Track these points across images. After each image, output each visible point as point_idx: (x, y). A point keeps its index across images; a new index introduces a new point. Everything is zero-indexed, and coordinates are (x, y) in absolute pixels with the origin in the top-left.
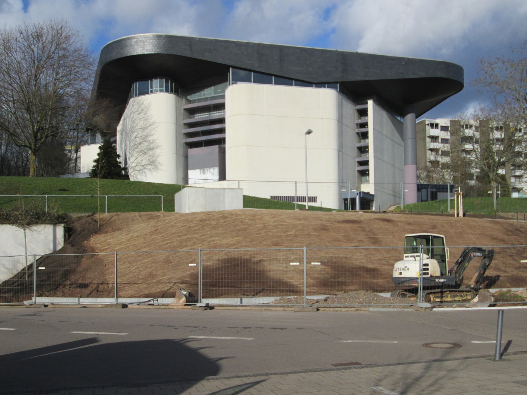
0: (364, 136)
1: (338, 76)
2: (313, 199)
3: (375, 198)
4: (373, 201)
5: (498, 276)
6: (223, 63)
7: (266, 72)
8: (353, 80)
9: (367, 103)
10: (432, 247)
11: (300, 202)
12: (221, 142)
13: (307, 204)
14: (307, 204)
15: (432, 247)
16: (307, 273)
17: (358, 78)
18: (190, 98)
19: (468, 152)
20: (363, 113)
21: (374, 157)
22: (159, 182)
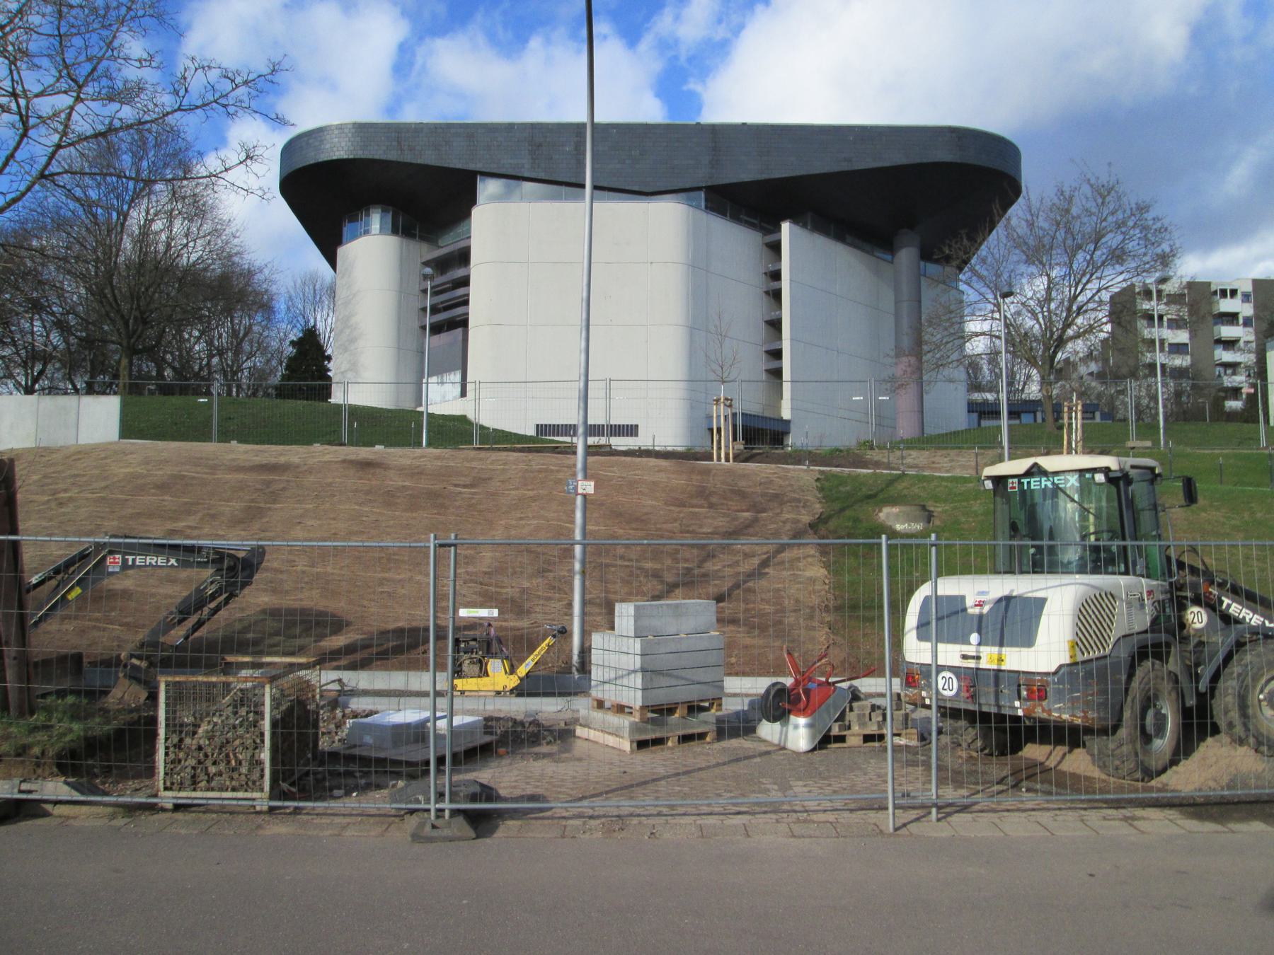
0: (776, 295)
1: (702, 176)
2: (631, 430)
3: (792, 426)
4: (787, 433)
5: (259, 553)
6: (459, 166)
7: (547, 178)
8: (735, 181)
9: (779, 229)
10: (1052, 543)
11: (558, 435)
12: (463, 323)
13: (620, 443)
14: (620, 443)
15: (1052, 543)
16: (588, 597)
17: (746, 177)
18: (441, 243)
19: (1230, 344)
20: (776, 248)
21: (791, 339)
22: (499, 427)
